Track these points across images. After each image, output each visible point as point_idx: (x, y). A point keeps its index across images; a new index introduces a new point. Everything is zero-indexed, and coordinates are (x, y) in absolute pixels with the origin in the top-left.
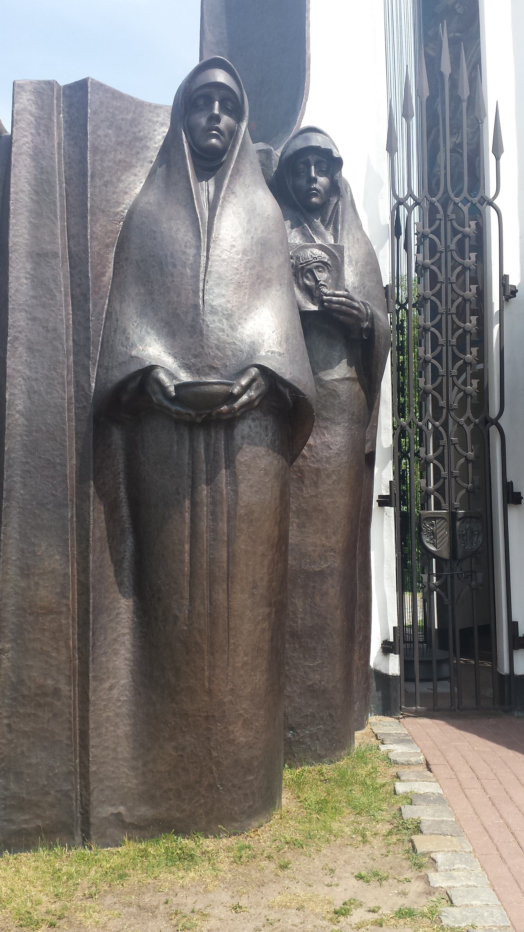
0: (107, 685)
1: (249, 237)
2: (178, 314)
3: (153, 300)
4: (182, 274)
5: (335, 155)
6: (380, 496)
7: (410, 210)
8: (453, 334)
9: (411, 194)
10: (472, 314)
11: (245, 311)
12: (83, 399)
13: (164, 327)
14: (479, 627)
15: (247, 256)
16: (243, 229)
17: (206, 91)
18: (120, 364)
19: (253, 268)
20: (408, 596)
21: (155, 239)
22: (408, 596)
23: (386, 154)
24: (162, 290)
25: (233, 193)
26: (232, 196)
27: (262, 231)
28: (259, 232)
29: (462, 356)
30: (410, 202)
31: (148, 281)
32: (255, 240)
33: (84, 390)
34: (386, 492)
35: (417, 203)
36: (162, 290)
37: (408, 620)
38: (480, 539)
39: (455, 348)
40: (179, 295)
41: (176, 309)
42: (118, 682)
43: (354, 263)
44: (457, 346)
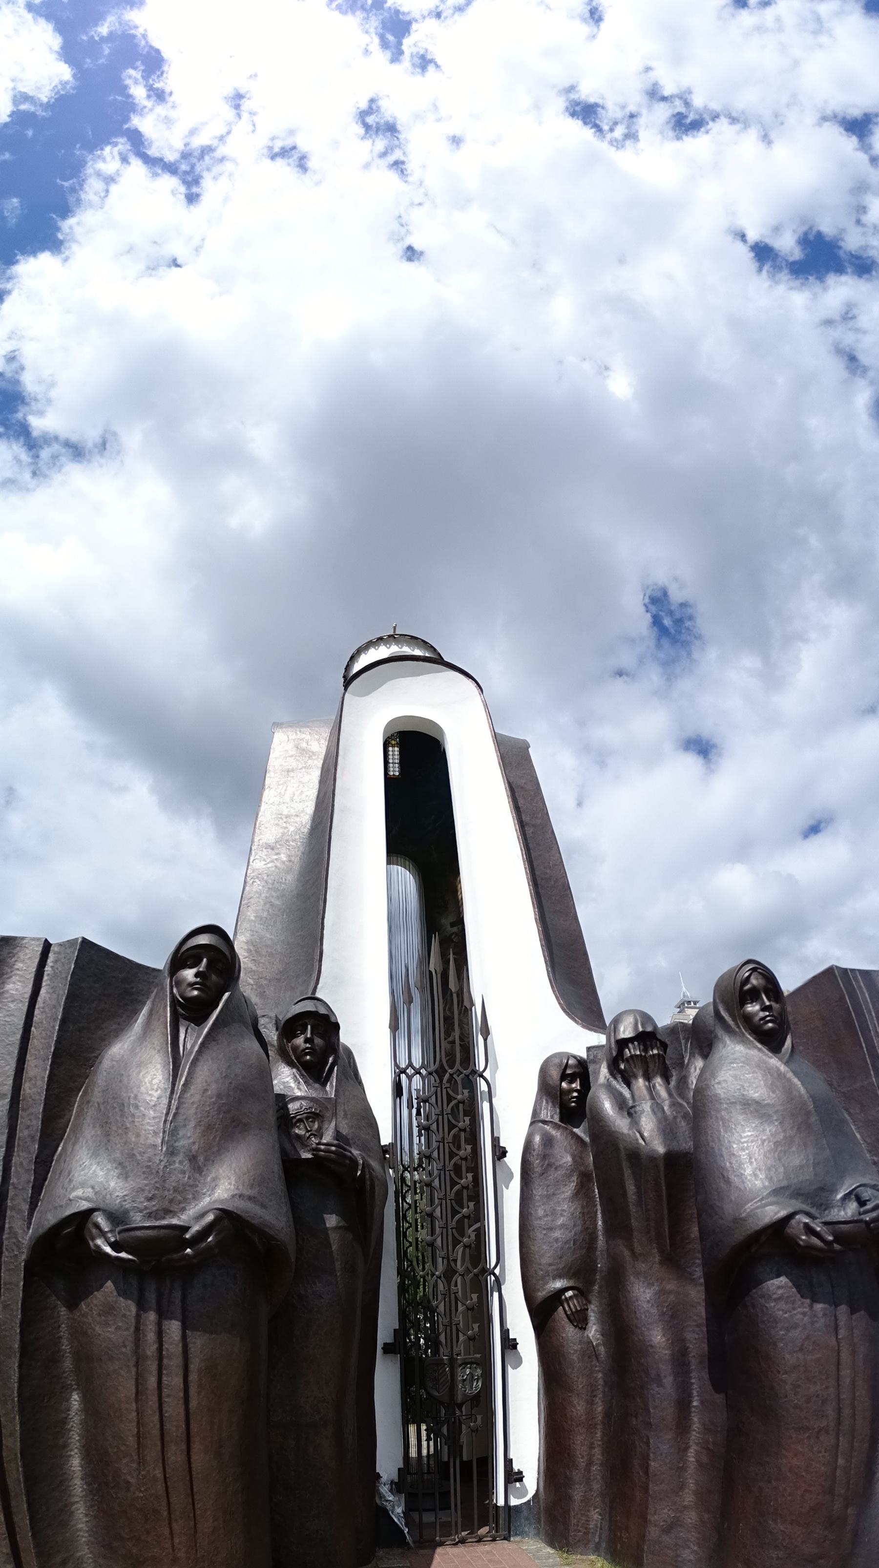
0: (58, 1559)
1: (227, 1082)
2: (134, 1155)
3: (109, 1141)
4: (144, 1115)
5: (333, 1020)
6: (385, 1344)
7: (410, 1078)
8: (453, 1218)
9: (410, 1065)
10: (470, 1199)
11: (213, 1153)
12: (14, 1248)
13: (116, 1168)
14: (477, 1459)
15: (222, 1099)
16: (221, 1073)
17: (195, 951)
18: (56, 1208)
19: (228, 1111)
20: (412, 1429)
21: (120, 1081)
22: (412, 1429)
23: (387, 1032)
24: (120, 1131)
25: (214, 1040)
26: (214, 1043)
27: (243, 1078)
28: (240, 1078)
29: (460, 1210)
30: (410, 1071)
31: (107, 1123)
32: (233, 1086)
33: (16, 1238)
34: (390, 1340)
35: (418, 1072)
36: (120, 1131)
37: (413, 1453)
38: (480, 1384)
39: (453, 1202)
40: (138, 1136)
41: (132, 1149)
42: (72, 1555)
43: (349, 1116)
44: (453, 1143)
